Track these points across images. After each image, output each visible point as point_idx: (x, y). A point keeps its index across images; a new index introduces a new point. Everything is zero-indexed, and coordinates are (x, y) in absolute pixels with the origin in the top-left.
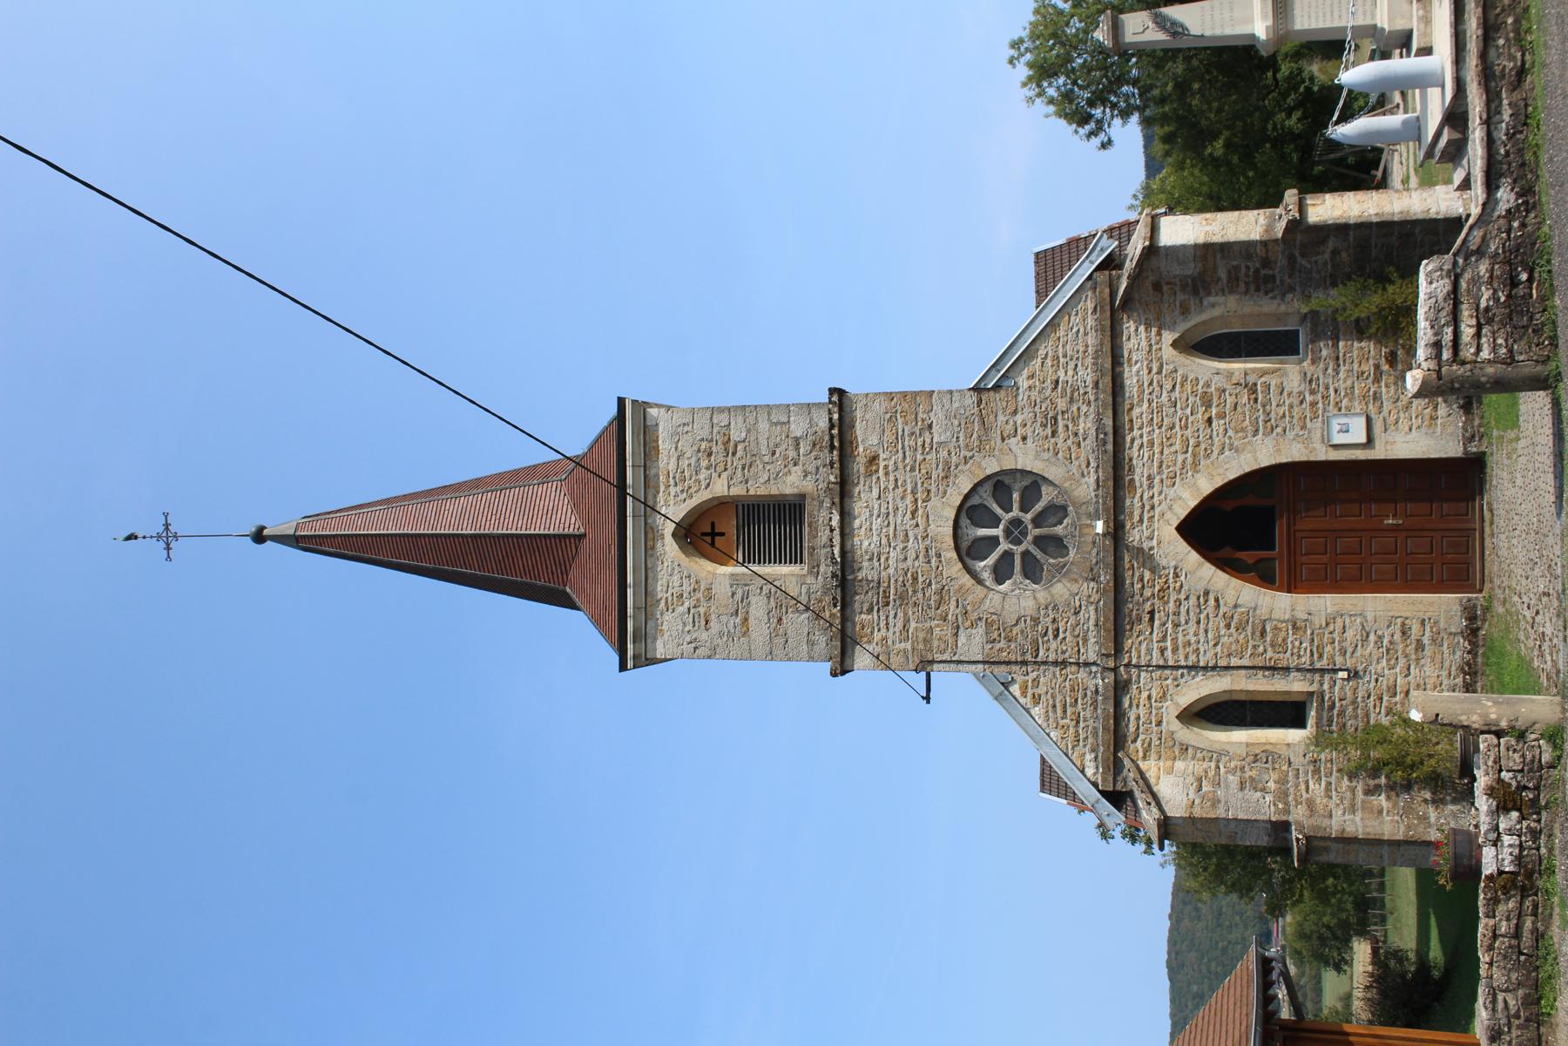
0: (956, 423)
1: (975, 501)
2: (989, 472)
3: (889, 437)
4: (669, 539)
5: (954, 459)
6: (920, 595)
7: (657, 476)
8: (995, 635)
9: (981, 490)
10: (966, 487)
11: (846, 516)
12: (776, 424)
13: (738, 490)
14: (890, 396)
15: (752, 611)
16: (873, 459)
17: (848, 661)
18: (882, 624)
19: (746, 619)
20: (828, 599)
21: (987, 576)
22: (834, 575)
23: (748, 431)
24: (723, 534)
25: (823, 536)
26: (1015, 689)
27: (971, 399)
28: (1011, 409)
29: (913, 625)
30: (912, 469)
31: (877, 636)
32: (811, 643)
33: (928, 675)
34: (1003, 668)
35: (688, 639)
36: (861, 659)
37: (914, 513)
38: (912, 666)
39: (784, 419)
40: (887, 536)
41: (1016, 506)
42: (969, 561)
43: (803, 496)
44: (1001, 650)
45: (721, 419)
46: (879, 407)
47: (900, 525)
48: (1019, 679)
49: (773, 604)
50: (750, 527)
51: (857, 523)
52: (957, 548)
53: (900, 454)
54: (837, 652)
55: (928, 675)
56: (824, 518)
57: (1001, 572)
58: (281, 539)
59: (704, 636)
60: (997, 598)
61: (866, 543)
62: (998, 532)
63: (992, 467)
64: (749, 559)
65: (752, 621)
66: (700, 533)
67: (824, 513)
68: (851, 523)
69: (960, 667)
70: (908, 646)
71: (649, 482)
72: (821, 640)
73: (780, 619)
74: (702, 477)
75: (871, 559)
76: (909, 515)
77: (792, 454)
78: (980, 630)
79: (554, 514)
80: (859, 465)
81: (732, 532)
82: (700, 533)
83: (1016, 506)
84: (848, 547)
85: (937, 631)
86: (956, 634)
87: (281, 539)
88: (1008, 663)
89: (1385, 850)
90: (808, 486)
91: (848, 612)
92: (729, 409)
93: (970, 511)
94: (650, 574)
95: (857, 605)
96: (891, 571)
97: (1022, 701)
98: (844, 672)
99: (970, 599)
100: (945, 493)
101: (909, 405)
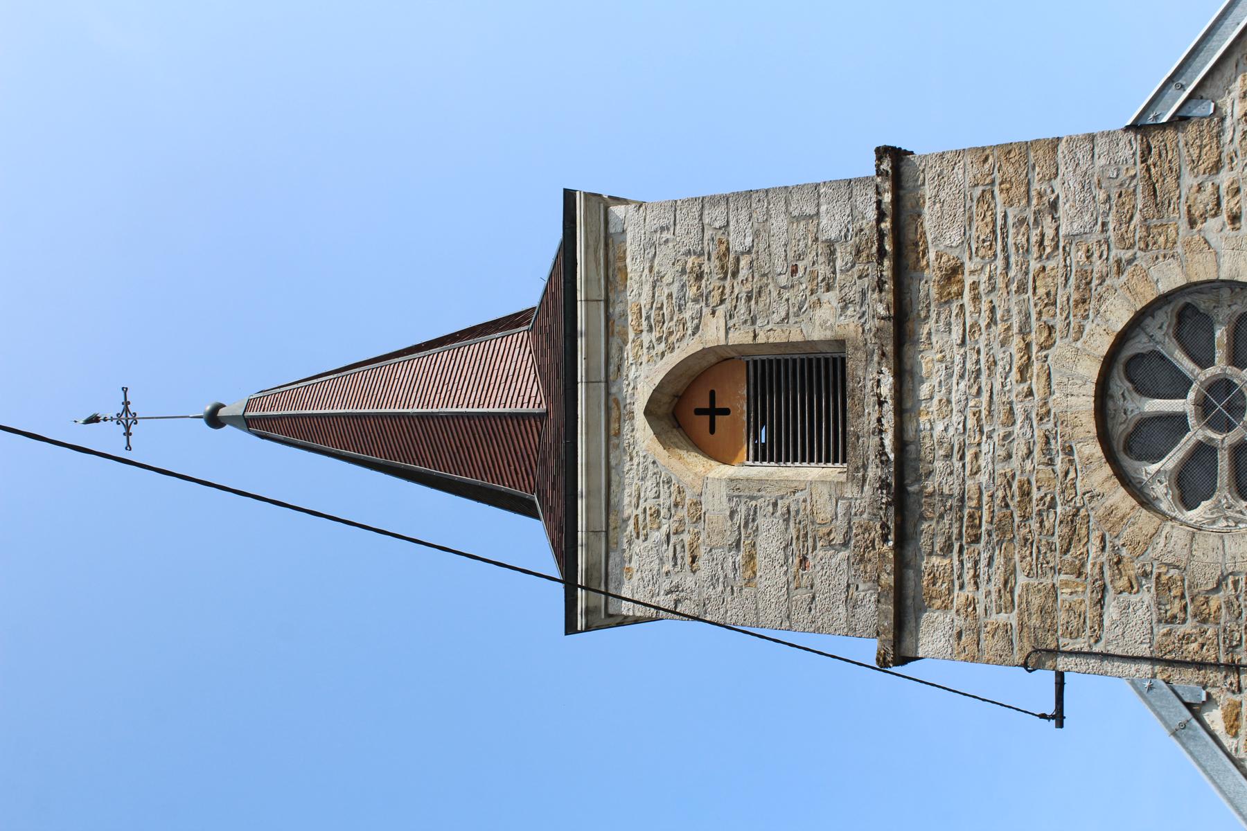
0: (1102, 196)
1: (1139, 345)
2: (1163, 288)
3: (980, 229)
4: (640, 420)
5: (1098, 265)
6: (1034, 525)
7: (624, 315)
8: (1176, 608)
9: (1152, 325)
10: (1120, 317)
11: (904, 375)
12: (797, 219)
13: (740, 337)
14: (983, 155)
15: (761, 541)
16: (953, 273)
17: (908, 642)
18: (968, 576)
19: (751, 557)
20: (876, 533)
21: (1161, 491)
22: (884, 484)
23: (756, 234)
24: (726, 412)
25: (872, 412)
26: (1215, 718)
27: (1128, 149)
28: (1209, 159)
29: (1022, 579)
30: (1022, 289)
31: (959, 598)
32: (852, 604)
33: (1060, 677)
34: (1189, 674)
35: (666, 586)
36: (933, 633)
37: (1024, 371)
38: (1018, 657)
39: (810, 210)
40: (977, 414)
41: (1220, 354)
42: (1128, 463)
43: (841, 343)
44: (1186, 638)
45: (715, 216)
46: (963, 175)
47: (1000, 393)
48: (1224, 698)
49: (793, 532)
50: (782, 399)
51: (924, 391)
52: (1104, 437)
53: (1000, 262)
54: (888, 623)
55: (1060, 677)
56: (873, 380)
57: (1191, 485)
58: (233, 420)
59: (689, 581)
60: (1179, 535)
61: (939, 427)
62: (1184, 405)
63: (1169, 277)
64: (762, 454)
65: (759, 557)
66: (687, 410)
67: (873, 368)
68: (914, 391)
69: (1107, 665)
70: (1013, 618)
71: (612, 327)
72: (867, 595)
73: (804, 560)
74: (687, 315)
75: (948, 456)
76: (1015, 376)
77: (823, 270)
78: (1147, 596)
79: (510, 384)
80: (928, 286)
81: (740, 407)
82: (687, 410)
83: (1220, 354)
84: (910, 434)
85: (1064, 594)
86: (1101, 603)
87: (233, 420)
88: (1201, 665)
89: (1226, 293)
90: (848, 326)
91: (909, 551)
92: (727, 199)
93: (1126, 364)
94: (614, 477)
95: (924, 540)
96: (983, 478)
97: (1229, 742)
98: (903, 660)
99: (1127, 533)
100: (1081, 330)
101: (1017, 166)
